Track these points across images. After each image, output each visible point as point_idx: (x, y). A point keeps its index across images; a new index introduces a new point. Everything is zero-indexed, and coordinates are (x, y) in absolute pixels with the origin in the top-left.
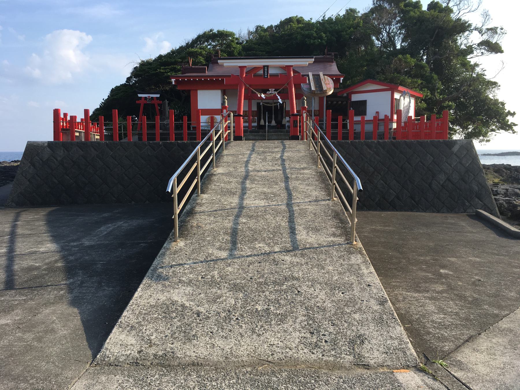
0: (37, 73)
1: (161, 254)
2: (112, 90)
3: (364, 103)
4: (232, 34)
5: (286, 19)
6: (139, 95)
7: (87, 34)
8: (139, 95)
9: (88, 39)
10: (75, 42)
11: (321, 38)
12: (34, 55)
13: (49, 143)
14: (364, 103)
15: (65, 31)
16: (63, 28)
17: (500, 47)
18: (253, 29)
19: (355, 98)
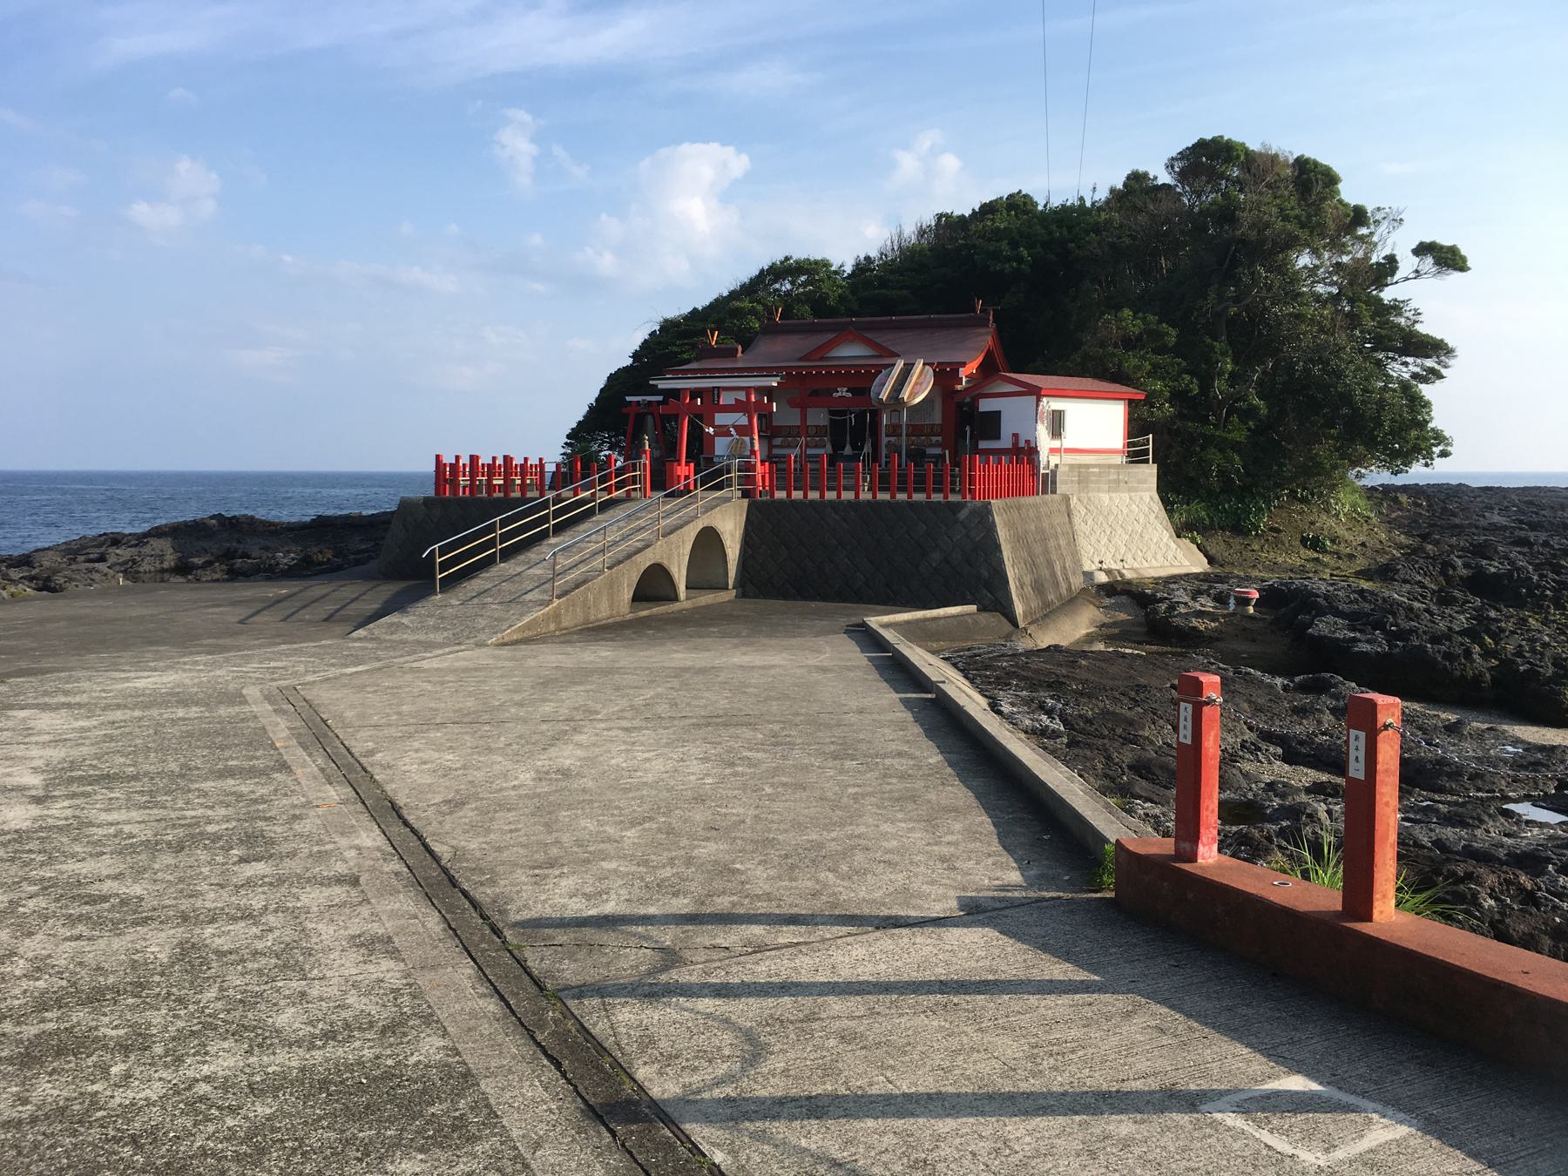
0: (606, 263)
1: (392, 624)
2: (611, 378)
3: (996, 416)
4: (825, 264)
5: (983, 206)
6: (628, 399)
7: (739, 151)
8: (628, 399)
9: (739, 163)
10: (707, 172)
11: (1020, 260)
12: (604, 217)
13: (427, 501)
14: (996, 416)
15: (686, 148)
16: (678, 141)
17: (1464, 259)
18: (929, 220)
19: (986, 405)
